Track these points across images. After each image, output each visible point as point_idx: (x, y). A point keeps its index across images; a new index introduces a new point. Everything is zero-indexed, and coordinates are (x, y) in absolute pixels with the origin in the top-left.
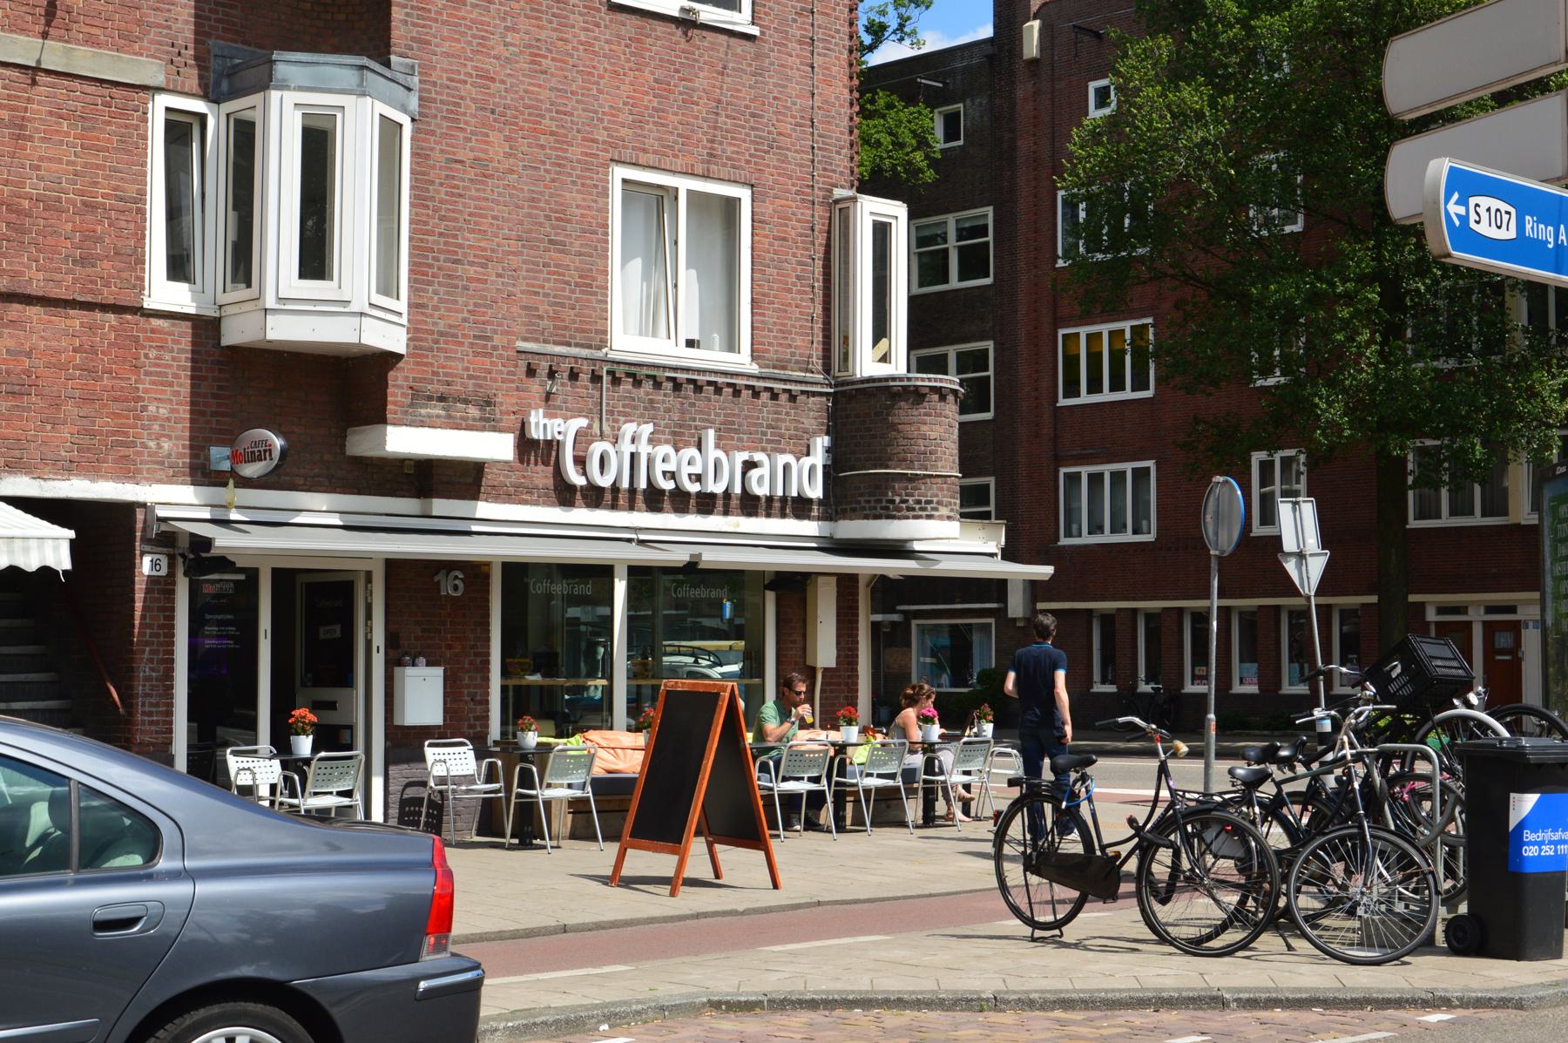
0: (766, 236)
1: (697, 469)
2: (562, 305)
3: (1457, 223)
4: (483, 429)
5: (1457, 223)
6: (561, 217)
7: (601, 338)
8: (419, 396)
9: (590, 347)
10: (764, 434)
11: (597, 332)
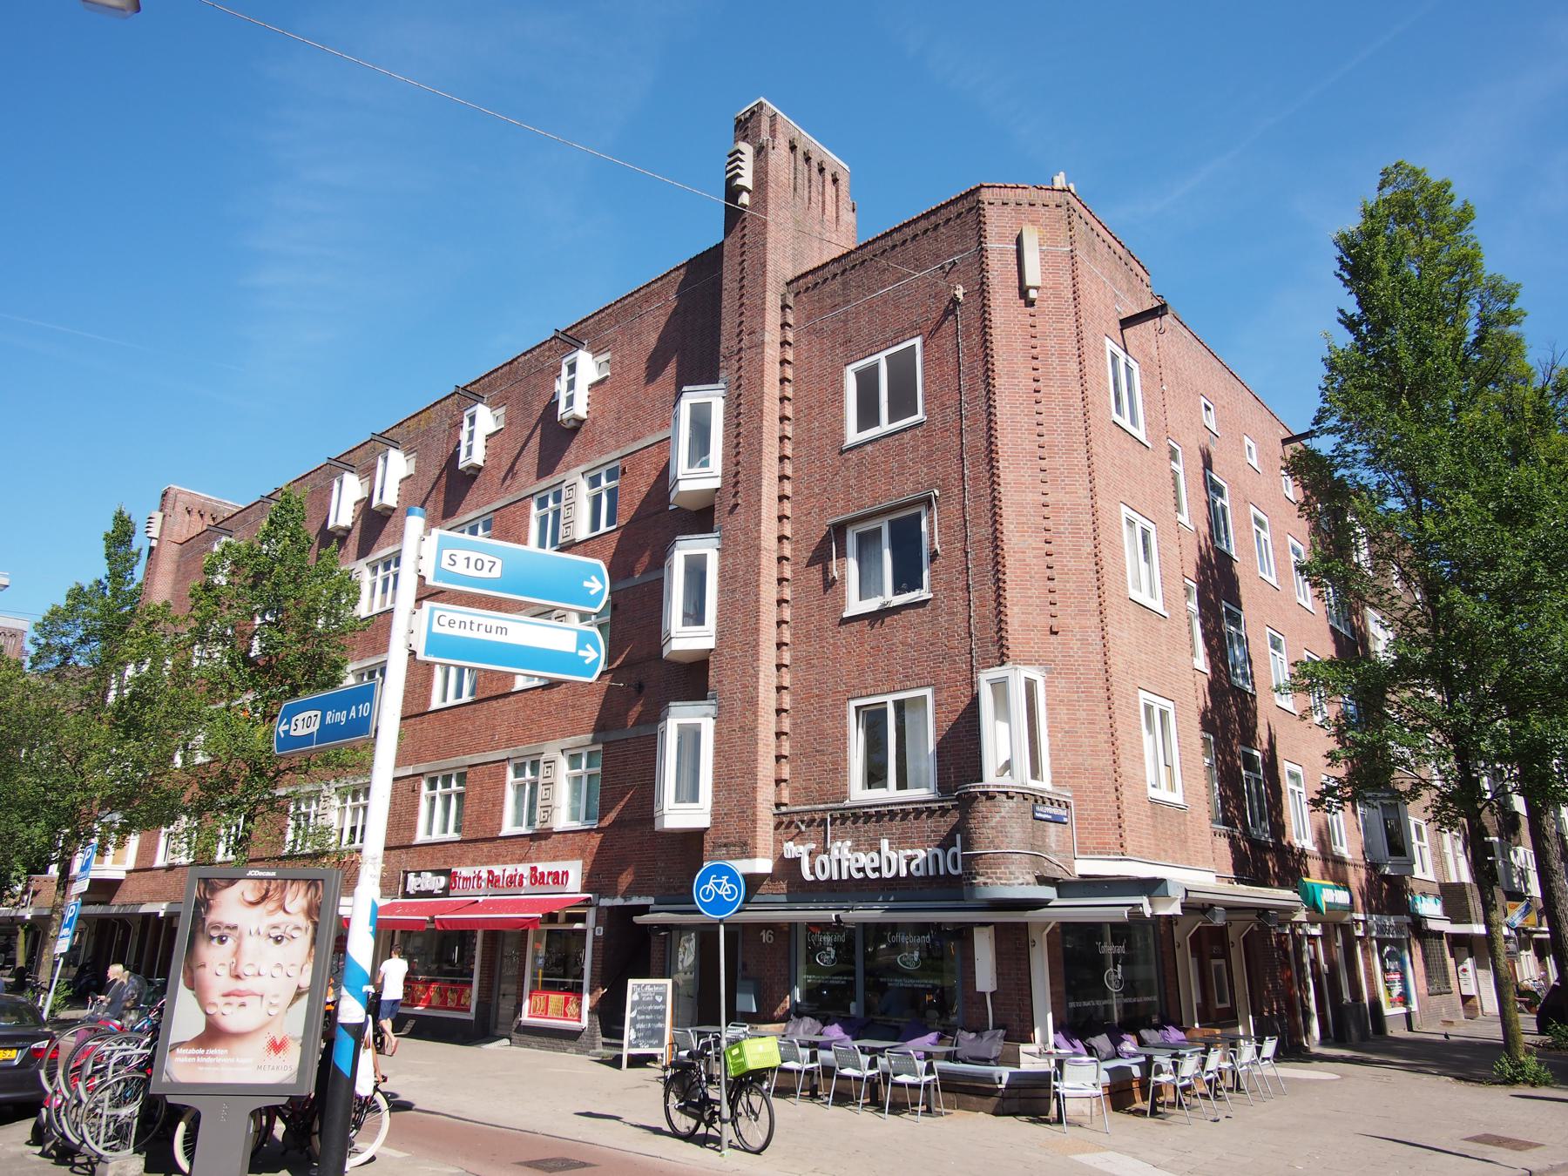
0: (944, 712)
1: (876, 864)
2: (823, 783)
3: (282, 735)
4: (741, 858)
5: (282, 735)
6: (822, 734)
7: (845, 795)
8: (716, 846)
9: (838, 802)
10: (928, 837)
11: (841, 793)
